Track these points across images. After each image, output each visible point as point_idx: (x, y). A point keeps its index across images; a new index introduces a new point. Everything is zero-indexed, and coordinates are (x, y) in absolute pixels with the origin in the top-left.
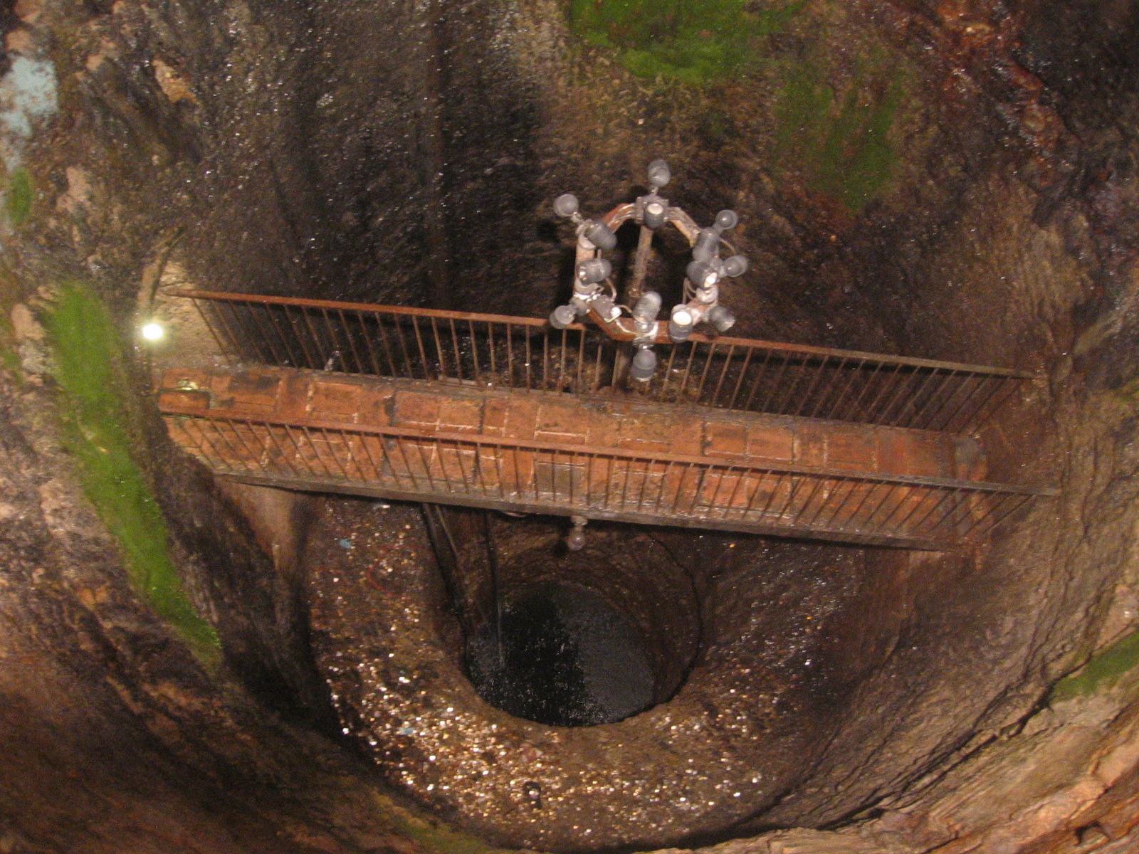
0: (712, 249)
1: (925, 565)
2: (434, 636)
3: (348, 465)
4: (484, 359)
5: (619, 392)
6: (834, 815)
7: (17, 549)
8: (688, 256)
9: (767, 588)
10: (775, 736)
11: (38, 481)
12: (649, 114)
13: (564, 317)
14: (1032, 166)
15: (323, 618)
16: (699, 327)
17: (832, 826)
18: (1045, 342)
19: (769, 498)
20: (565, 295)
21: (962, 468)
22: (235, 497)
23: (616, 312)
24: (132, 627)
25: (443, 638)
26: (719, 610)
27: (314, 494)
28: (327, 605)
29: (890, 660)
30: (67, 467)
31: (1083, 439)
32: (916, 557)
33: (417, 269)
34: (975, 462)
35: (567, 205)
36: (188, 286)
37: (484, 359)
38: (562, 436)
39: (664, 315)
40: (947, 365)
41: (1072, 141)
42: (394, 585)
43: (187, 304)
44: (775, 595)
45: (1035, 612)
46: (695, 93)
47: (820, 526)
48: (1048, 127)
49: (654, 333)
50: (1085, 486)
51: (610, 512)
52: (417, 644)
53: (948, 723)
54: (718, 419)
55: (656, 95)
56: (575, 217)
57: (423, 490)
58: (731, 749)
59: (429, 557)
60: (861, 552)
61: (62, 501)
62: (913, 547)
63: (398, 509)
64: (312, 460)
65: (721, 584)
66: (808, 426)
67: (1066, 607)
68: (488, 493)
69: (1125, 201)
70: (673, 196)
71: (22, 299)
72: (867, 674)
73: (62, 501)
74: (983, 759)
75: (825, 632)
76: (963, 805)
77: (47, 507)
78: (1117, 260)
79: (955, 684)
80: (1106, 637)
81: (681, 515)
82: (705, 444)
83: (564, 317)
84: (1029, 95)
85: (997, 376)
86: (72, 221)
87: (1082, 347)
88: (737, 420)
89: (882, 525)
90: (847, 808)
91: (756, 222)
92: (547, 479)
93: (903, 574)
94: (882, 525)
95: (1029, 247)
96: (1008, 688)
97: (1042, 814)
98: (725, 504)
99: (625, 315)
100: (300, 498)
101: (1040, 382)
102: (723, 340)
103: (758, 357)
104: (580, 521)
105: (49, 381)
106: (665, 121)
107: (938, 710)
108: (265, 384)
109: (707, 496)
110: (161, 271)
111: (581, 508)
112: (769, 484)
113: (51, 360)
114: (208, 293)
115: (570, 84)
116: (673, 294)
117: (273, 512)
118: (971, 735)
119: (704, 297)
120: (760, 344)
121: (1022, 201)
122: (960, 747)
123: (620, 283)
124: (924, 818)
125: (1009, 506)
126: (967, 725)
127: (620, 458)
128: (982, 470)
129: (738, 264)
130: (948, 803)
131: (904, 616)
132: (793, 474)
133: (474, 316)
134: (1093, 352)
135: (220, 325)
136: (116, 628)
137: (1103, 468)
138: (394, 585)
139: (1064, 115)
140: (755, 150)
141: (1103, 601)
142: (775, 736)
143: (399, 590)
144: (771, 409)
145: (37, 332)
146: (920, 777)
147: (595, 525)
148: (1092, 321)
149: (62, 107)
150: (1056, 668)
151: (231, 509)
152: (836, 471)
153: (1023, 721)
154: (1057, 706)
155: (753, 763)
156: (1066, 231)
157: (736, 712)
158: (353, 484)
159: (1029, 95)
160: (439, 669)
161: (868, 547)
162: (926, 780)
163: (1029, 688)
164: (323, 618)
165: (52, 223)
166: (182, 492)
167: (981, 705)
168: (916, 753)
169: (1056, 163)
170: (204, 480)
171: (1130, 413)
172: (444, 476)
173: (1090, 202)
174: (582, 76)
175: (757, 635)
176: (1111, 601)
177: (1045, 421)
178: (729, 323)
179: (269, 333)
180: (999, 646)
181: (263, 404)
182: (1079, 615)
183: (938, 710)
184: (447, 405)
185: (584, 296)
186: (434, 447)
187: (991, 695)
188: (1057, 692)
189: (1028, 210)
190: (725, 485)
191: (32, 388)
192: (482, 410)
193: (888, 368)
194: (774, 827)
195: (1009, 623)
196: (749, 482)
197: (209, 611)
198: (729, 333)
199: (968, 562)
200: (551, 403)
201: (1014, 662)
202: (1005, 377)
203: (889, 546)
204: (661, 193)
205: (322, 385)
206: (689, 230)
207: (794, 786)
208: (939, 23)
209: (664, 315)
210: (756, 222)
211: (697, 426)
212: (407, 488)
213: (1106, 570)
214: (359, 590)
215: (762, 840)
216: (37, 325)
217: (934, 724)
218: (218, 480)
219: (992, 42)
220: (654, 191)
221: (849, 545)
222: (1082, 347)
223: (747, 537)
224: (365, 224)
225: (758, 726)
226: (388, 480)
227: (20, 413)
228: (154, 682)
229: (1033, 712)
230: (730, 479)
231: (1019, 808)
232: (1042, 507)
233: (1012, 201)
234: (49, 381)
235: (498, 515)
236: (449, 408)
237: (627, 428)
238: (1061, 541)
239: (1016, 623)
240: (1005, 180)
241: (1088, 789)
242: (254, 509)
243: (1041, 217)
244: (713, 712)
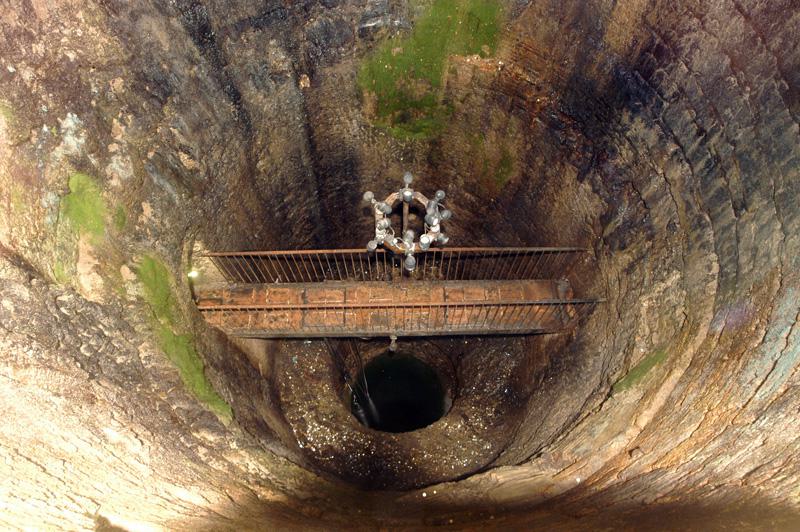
0: (435, 208)
1: (552, 342)
2: (337, 398)
3: (287, 323)
4: (344, 273)
5: (405, 278)
6: (523, 459)
7: (127, 376)
8: (424, 213)
9: (484, 360)
10: (495, 426)
11: (136, 344)
12: (405, 154)
13: (373, 245)
14: (574, 156)
15: (286, 396)
16: (432, 245)
17: (520, 464)
18: (590, 234)
19: (476, 318)
20: (373, 236)
21: (561, 295)
22: (238, 344)
23: (395, 241)
24: (186, 406)
25: (341, 398)
26: (463, 372)
27: (277, 339)
28: (288, 389)
29: (541, 385)
30: (150, 337)
31: (613, 276)
32: (547, 337)
33: (311, 235)
34: (567, 292)
35: (368, 196)
36: (206, 252)
37: (344, 273)
38: (382, 301)
39: (417, 240)
40: (548, 249)
41: (589, 143)
42: (317, 377)
43: (207, 260)
44: (488, 362)
45: (602, 355)
46: (424, 144)
47: (501, 328)
48: (579, 138)
49: (413, 249)
50: (616, 296)
51: (406, 332)
52: (330, 403)
53: (570, 410)
54: (451, 286)
55: (407, 146)
56: (373, 201)
57: (322, 332)
58: (477, 434)
59: (331, 362)
60: (523, 338)
61: (149, 352)
62: (544, 333)
63: (316, 343)
64: (271, 324)
65: (463, 360)
66: (489, 284)
67: (615, 350)
68: (350, 330)
69: (616, 166)
70: (414, 187)
71: (124, 262)
72: (532, 393)
73: (149, 352)
74: (584, 424)
75: (512, 376)
76: (577, 447)
77: (142, 356)
78: (616, 193)
79: (570, 392)
80: (634, 361)
81: (439, 329)
82: (446, 297)
83: (373, 245)
84: (568, 126)
85: (571, 252)
86: (147, 226)
87: (607, 232)
88: (459, 285)
89: (529, 324)
90: (528, 455)
91: (458, 197)
92: (376, 319)
93: (543, 346)
94: (529, 324)
95: (578, 192)
96: (594, 391)
97: (613, 446)
98: (460, 322)
99: (400, 242)
100: (270, 342)
101: (591, 252)
102: (445, 249)
103: (464, 256)
104: (394, 338)
105: (140, 299)
106: (412, 157)
107: (565, 405)
108: (247, 292)
109: (449, 320)
110: (192, 246)
111: (394, 333)
112: (476, 311)
113: (140, 289)
114: (216, 254)
115: (369, 145)
116: (420, 231)
117: (258, 350)
118: (579, 415)
119: (434, 229)
120: (464, 249)
121: (570, 177)
122: (576, 419)
123: (398, 229)
124: (560, 455)
125: (586, 307)
126: (577, 410)
127: (407, 307)
128: (571, 294)
129: (446, 214)
130: (571, 446)
131: (545, 364)
132: (485, 305)
133: (335, 251)
134: (611, 234)
135: (223, 269)
136: (178, 408)
137: (623, 286)
138: (317, 377)
139: (583, 131)
140: (453, 166)
141: (631, 344)
142: (495, 426)
143: (319, 379)
144: (474, 278)
145: (133, 277)
146: (559, 436)
147: (401, 339)
148: (609, 222)
149: (137, 174)
150: (614, 379)
151: (237, 349)
152: (504, 302)
153: (601, 405)
154: (615, 395)
155: (487, 439)
156: (592, 183)
157: (476, 417)
158: (291, 333)
159: (568, 126)
160: (341, 413)
161: (525, 335)
162: (561, 437)
163: (603, 390)
164: (286, 396)
165: (137, 228)
166: (215, 347)
167: (583, 400)
168: (557, 426)
169: (583, 153)
170: (222, 337)
171: (631, 260)
172: (331, 323)
173: (601, 169)
174: (374, 142)
175: (482, 381)
176: (634, 345)
177: (595, 267)
178: (446, 240)
179: (248, 271)
180: (589, 372)
181: (247, 302)
182: (621, 354)
183: (565, 405)
184: (328, 293)
185: (381, 235)
186: (325, 312)
187: (587, 396)
188: (615, 389)
189: (575, 176)
190: (456, 314)
191: (132, 303)
192: (345, 293)
193: (522, 254)
194: (494, 467)
195: (591, 362)
196: (467, 311)
197: (229, 397)
198: (447, 245)
199: (570, 336)
200: (375, 286)
201: (595, 380)
202: (574, 251)
203: (533, 334)
204: (410, 186)
205: (272, 290)
206: (424, 201)
207: (505, 447)
208: (525, 99)
209: (417, 240)
210: (458, 197)
211: (441, 291)
212: (314, 332)
213: (630, 331)
214: (302, 381)
215: (487, 474)
216: (133, 274)
217: (563, 410)
218: (229, 338)
219: (549, 104)
220: (407, 185)
221: (517, 335)
222: (607, 232)
223: (472, 337)
224: (285, 217)
225: (487, 421)
226: (306, 329)
227: (127, 315)
228: (198, 432)
229: (606, 400)
230: (458, 312)
231: (603, 445)
232: (599, 307)
233: (567, 173)
234: (140, 299)
235: (359, 339)
236: (332, 293)
237: (408, 294)
238: (609, 322)
239: (594, 361)
240: (563, 164)
241: (633, 432)
242: (248, 349)
243: (580, 178)
244: (466, 418)
